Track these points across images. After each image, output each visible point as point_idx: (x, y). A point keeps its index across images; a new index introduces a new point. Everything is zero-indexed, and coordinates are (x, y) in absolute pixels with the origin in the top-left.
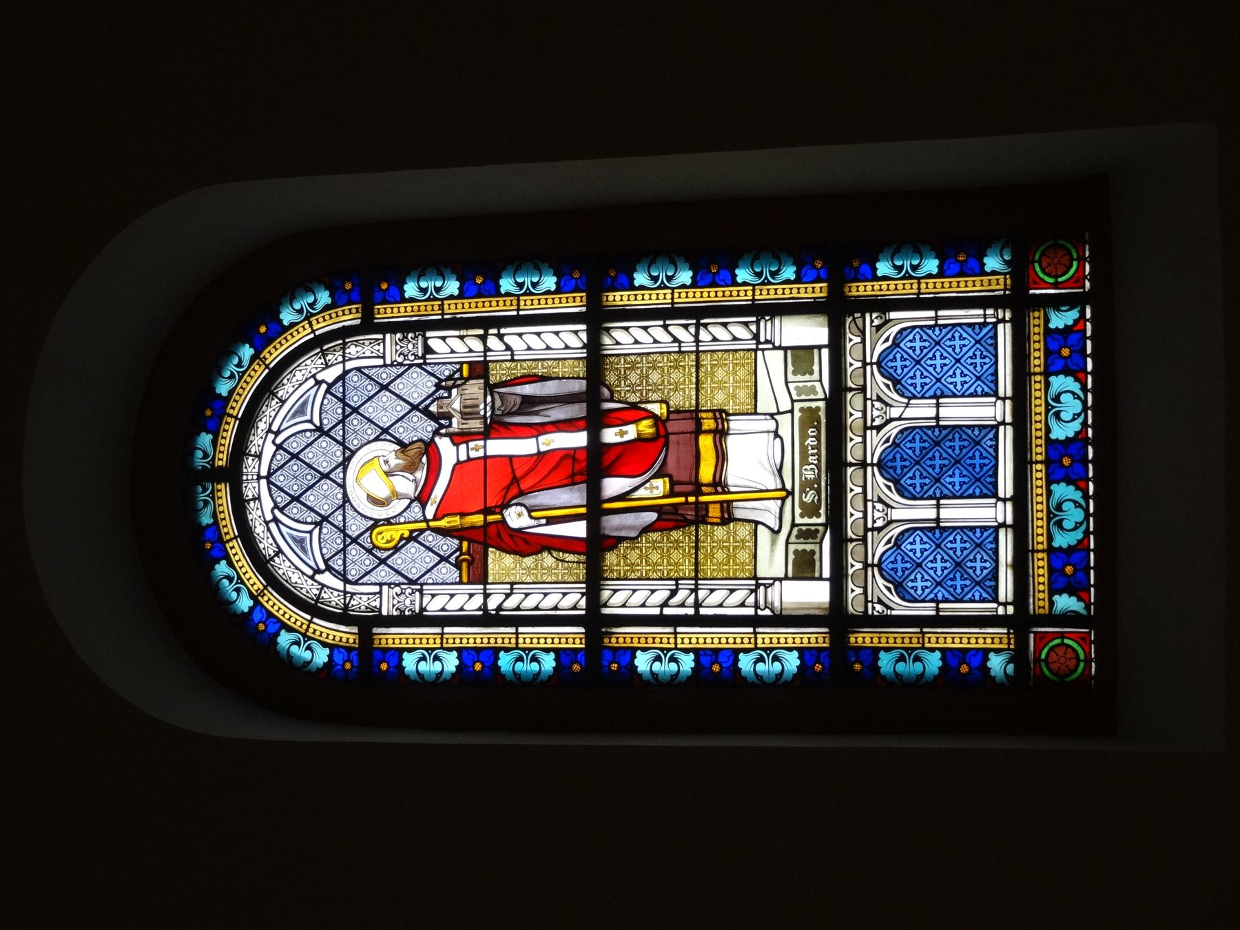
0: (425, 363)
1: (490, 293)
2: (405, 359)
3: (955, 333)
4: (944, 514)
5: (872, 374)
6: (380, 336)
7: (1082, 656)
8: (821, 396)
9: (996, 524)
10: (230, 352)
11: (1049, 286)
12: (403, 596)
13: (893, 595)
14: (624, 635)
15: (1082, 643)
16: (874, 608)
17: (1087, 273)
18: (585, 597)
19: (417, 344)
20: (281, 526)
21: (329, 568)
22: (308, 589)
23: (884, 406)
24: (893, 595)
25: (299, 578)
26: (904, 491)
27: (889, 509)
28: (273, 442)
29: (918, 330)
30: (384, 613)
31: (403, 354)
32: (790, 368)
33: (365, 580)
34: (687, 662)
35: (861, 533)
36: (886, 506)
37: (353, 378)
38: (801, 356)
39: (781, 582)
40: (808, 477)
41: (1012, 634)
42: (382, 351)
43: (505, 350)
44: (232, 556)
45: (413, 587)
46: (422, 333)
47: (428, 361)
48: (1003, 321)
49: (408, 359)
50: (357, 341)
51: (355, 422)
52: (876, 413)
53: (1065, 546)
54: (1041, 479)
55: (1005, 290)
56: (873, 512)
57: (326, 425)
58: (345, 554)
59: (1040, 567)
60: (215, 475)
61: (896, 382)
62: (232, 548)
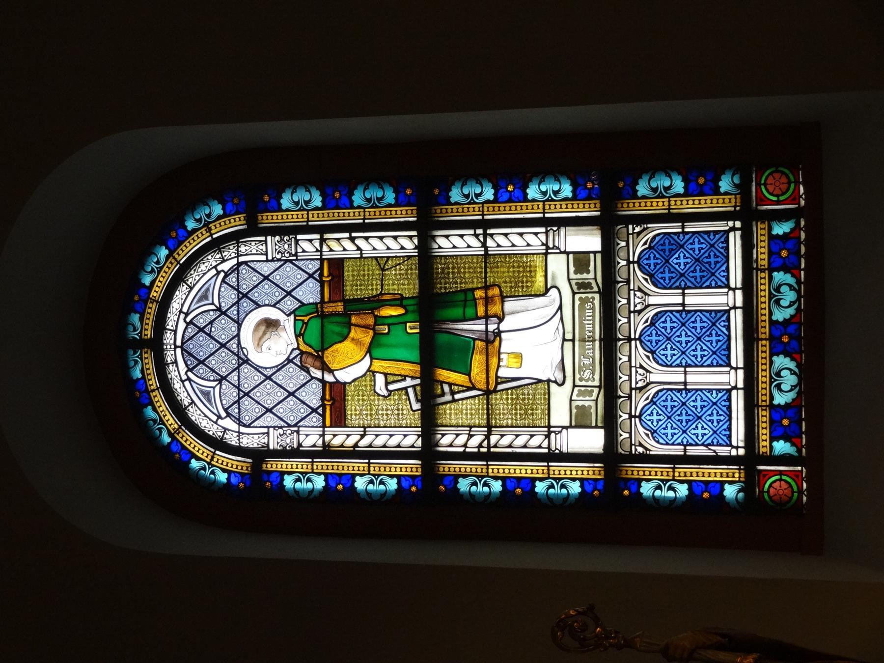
0: (297, 260)
1: (346, 206)
2: (282, 257)
3: (698, 424)
4: (688, 300)
5: (634, 270)
6: (263, 238)
7: (795, 489)
8: (596, 289)
9: (729, 387)
10: (149, 252)
11: (773, 203)
12: (285, 436)
13: (650, 439)
14: (449, 467)
15: (796, 479)
16: (636, 450)
17: (804, 476)
18: (421, 438)
19: (291, 245)
20: (192, 382)
21: (229, 415)
22: (212, 430)
23: (643, 295)
24: (650, 439)
25: (208, 423)
26: (657, 283)
27: (648, 374)
28: (185, 321)
29: (669, 313)
30: (271, 447)
31: (281, 252)
32: (572, 269)
33: (255, 424)
34: (497, 486)
35: (628, 392)
36: (645, 449)
37: (243, 269)
38: (581, 260)
39: (567, 430)
40: (585, 362)
41: (742, 469)
42: (264, 250)
43: (357, 250)
44: (155, 403)
45: (292, 429)
46: (294, 236)
47: (299, 258)
48: (734, 229)
49: (285, 256)
50: (245, 242)
51: (246, 403)
52: (638, 301)
53: (783, 403)
54: (766, 434)
55: (735, 207)
56: (636, 375)
57: (224, 307)
58: (238, 306)
59: (763, 417)
60: (141, 344)
61: (651, 276)
62: (155, 397)
